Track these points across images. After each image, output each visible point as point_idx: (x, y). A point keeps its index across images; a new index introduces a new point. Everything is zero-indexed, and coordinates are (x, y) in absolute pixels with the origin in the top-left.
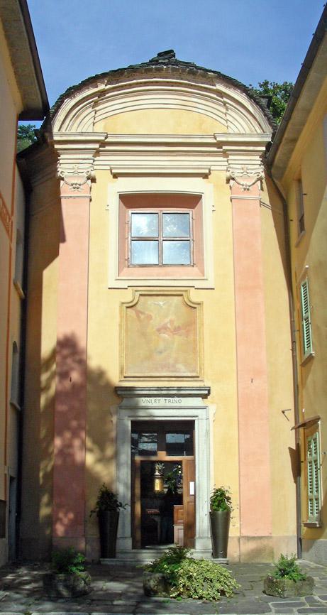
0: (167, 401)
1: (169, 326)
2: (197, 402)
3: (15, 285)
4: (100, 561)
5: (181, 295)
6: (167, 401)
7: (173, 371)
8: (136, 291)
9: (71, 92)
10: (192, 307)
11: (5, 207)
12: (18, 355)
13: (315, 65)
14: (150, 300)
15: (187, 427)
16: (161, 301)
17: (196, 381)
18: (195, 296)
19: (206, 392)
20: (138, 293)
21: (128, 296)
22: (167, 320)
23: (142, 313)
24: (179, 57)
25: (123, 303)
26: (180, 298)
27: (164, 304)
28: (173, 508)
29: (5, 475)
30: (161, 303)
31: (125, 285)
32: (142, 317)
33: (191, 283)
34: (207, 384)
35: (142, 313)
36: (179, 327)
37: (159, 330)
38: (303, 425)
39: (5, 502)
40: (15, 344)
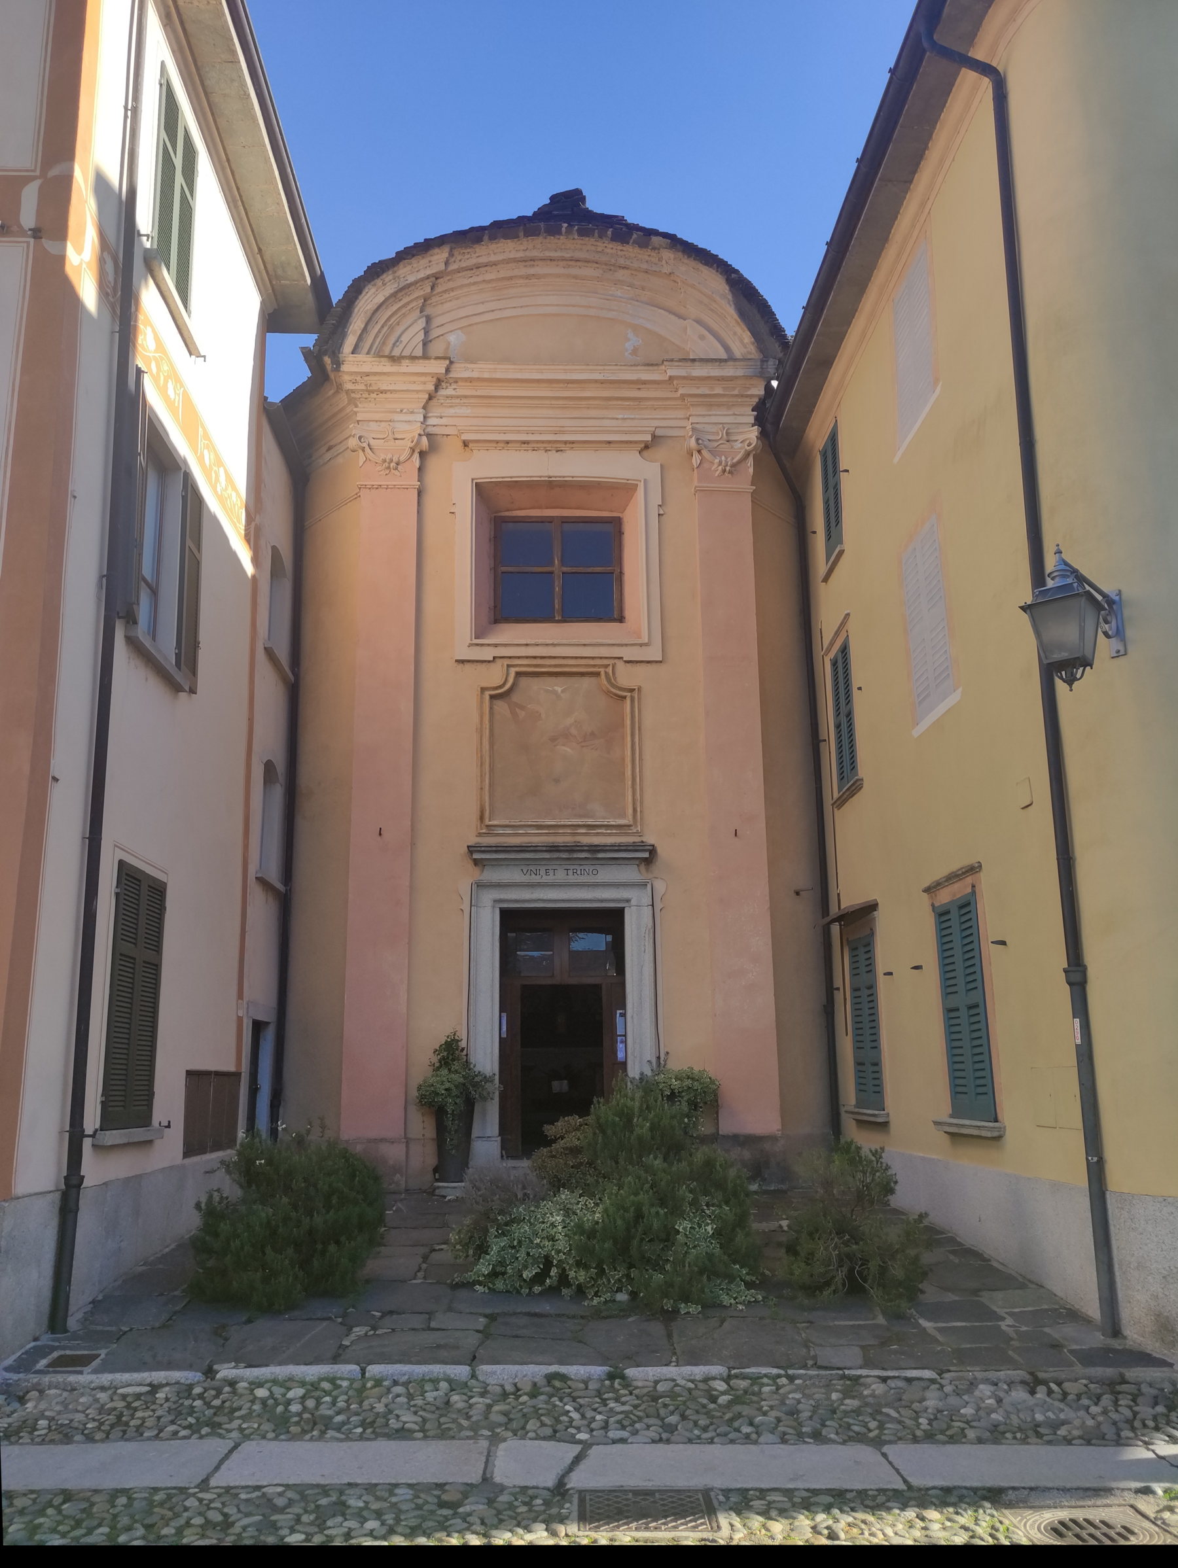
0: (570, 872)
1: (573, 731)
2: (630, 874)
3: (269, 652)
4: (432, 1192)
5: (598, 674)
6: (570, 872)
7: (580, 816)
8: (508, 666)
9: (376, 271)
10: (619, 695)
11: (234, 488)
12: (278, 792)
13: (686, 1484)
14: (535, 685)
15: (611, 921)
16: (558, 686)
17: (627, 834)
18: (626, 677)
19: (646, 855)
20: (513, 671)
21: (495, 676)
22: (570, 721)
23: (522, 708)
24: (595, 204)
25: (483, 690)
26: (593, 680)
27: (563, 691)
28: (17, 1550)
29: (240, 1020)
30: (559, 690)
31: (488, 654)
32: (522, 714)
33: (617, 652)
34: (650, 839)
35: (522, 708)
36: (592, 734)
37: (553, 739)
38: (839, 919)
39: (237, 1075)
40: (269, 767)
